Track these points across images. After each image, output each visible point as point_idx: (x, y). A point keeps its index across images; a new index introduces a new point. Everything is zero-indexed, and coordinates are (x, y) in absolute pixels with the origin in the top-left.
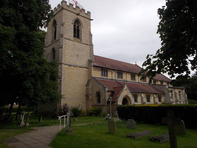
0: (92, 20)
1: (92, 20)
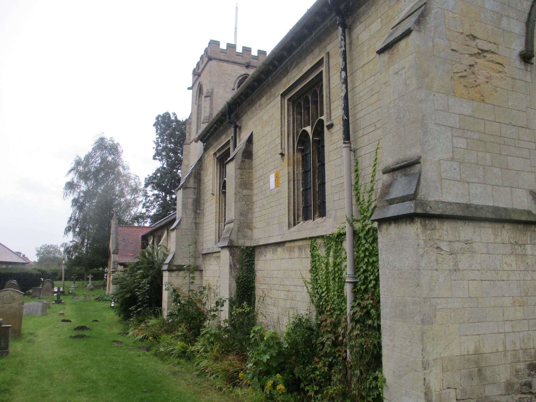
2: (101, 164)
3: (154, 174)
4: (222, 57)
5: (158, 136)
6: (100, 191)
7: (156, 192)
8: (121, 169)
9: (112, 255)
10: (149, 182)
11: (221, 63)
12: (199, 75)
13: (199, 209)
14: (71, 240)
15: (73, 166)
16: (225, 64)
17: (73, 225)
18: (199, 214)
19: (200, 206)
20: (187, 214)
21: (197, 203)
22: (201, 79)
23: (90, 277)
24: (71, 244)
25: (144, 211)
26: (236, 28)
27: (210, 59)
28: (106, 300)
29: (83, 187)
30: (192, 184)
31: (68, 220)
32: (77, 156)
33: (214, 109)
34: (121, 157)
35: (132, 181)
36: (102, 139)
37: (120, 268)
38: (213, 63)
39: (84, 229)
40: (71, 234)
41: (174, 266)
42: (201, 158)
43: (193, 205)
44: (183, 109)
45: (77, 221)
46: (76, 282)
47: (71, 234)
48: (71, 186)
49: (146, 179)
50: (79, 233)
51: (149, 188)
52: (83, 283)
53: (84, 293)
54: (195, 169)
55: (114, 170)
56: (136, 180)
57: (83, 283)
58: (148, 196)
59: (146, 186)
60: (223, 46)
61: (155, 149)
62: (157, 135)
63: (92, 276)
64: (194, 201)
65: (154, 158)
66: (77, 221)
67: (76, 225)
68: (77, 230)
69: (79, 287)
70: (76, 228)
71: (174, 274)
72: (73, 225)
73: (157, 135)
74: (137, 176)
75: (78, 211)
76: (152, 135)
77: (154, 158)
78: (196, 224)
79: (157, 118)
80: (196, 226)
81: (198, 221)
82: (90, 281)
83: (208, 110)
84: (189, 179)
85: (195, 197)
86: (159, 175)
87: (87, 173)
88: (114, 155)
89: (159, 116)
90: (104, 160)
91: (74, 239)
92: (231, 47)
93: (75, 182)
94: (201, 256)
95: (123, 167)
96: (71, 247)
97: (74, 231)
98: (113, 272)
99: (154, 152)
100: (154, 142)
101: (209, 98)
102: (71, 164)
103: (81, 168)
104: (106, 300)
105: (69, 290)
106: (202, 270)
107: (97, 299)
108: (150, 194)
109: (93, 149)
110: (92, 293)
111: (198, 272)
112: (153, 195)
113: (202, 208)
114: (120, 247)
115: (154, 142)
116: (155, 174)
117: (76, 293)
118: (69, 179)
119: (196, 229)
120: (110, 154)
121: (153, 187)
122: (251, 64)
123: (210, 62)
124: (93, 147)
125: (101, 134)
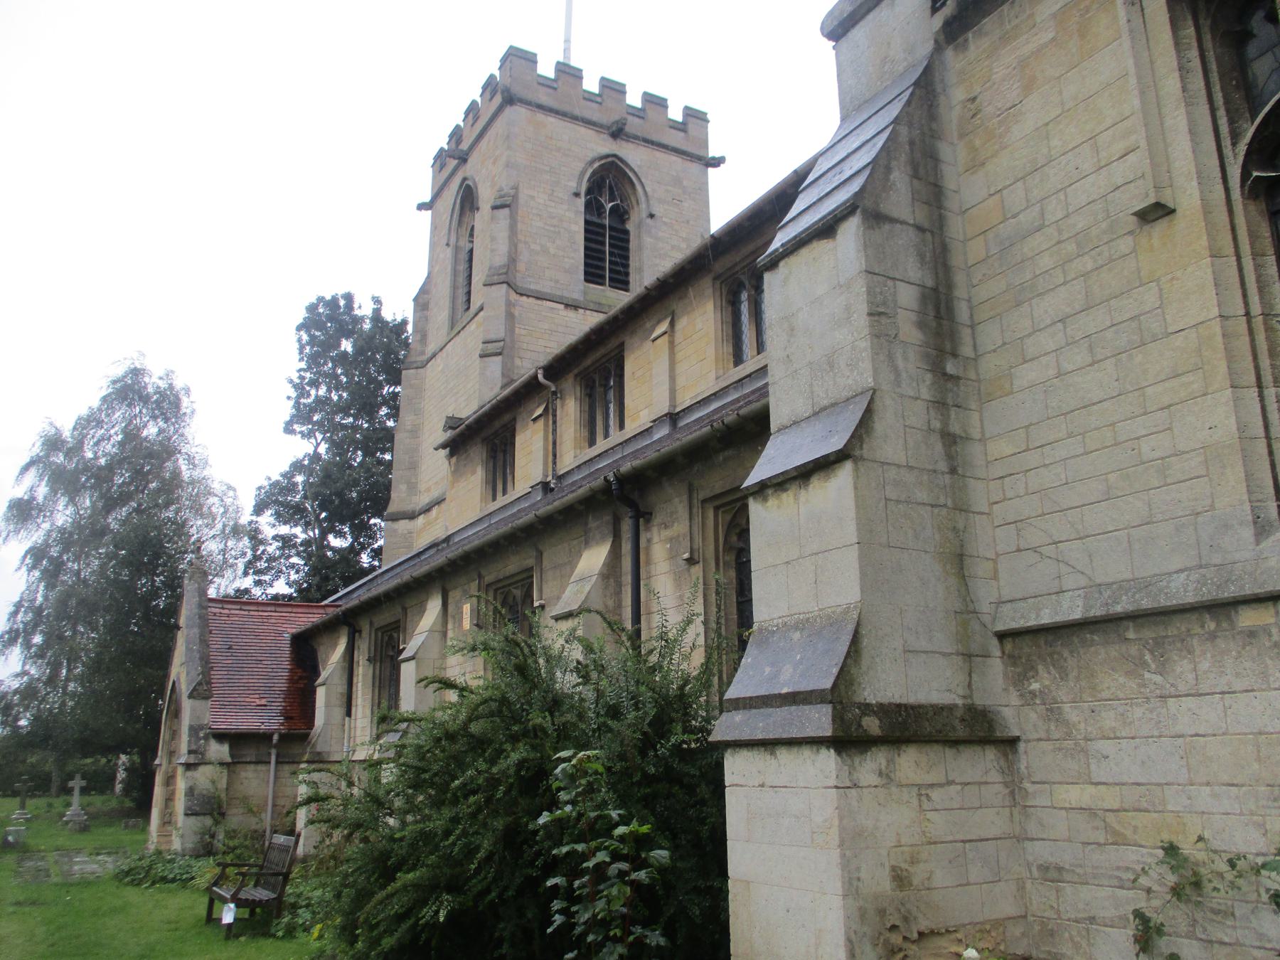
0: (717, 162)
1: (717, 162)
2: (122, 444)
3: (284, 475)
4: (544, 98)
5: (303, 365)
6: (114, 526)
7: (284, 530)
8: (183, 465)
9: (187, 705)
10: (274, 497)
11: (540, 116)
12: (463, 160)
13: (955, 355)
14: (18, 669)
15: (37, 450)
16: (551, 120)
17: (26, 624)
18: (955, 379)
19: (953, 336)
20: (897, 373)
21: (938, 317)
22: (469, 169)
23: (77, 783)
24: (16, 684)
25: (247, 582)
26: (567, 41)
27: (510, 100)
28: (164, 879)
29: (63, 515)
30: (900, 199)
31: (12, 609)
32: (51, 424)
33: (521, 246)
34: (187, 431)
35: (215, 500)
36: (136, 373)
37: (219, 751)
38: (517, 113)
39: (61, 638)
40: (16, 653)
41: (866, 708)
42: (928, 71)
43: (921, 325)
44: (391, 271)
45: (38, 611)
46: (31, 803)
47: (16, 653)
48: (23, 511)
49: (259, 488)
50: (40, 654)
51: (266, 519)
52: (50, 805)
53: (61, 841)
54: (910, 125)
55: (161, 467)
56: (228, 501)
57: (50, 805)
58: (262, 542)
59: (258, 510)
60: (546, 69)
61: (292, 403)
62: (301, 360)
63: (84, 783)
64: (924, 299)
65: (288, 429)
66: (38, 611)
67: (36, 625)
68: (38, 639)
69: (36, 817)
70: (33, 633)
71: (870, 765)
72: (26, 624)
73: (301, 360)
74: (230, 488)
75: (42, 588)
76: (284, 359)
77: (288, 429)
78: (951, 440)
79: (312, 308)
80: (950, 457)
81: (955, 428)
82: (76, 799)
83: (503, 247)
84: (888, 169)
85: (930, 283)
86: (299, 479)
87: (77, 473)
88: (166, 420)
89: (321, 299)
90: (131, 435)
91: (27, 667)
92: (569, 73)
93: (40, 499)
94: (994, 647)
95: (190, 460)
96: (16, 692)
97: (28, 645)
98: (189, 766)
99: (287, 410)
100: (291, 381)
101: (506, 211)
102: (30, 446)
103: (60, 458)
104: (164, 879)
105: (7, 833)
106: (1013, 742)
107: (127, 873)
108: (268, 532)
109: (104, 399)
110: (87, 841)
111: (991, 753)
112: (274, 538)
113: (966, 350)
114: (216, 675)
115: (291, 381)
116: (288, 476)
117: (32, 842)
118: (20, 492)
119: (953, 471)
120: (154, 418)
121: (278, 516)
122: (627, 129)
123: (509, 112)
124: (104, 393)
125: (135, 355)
